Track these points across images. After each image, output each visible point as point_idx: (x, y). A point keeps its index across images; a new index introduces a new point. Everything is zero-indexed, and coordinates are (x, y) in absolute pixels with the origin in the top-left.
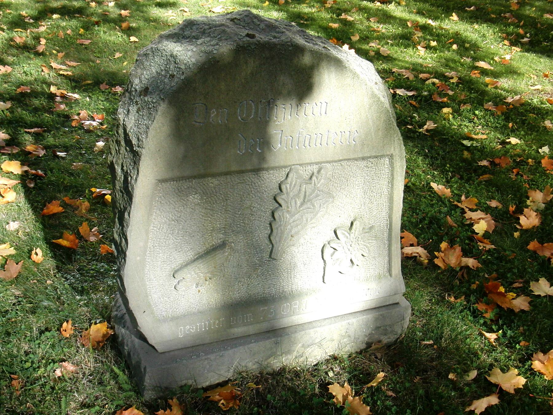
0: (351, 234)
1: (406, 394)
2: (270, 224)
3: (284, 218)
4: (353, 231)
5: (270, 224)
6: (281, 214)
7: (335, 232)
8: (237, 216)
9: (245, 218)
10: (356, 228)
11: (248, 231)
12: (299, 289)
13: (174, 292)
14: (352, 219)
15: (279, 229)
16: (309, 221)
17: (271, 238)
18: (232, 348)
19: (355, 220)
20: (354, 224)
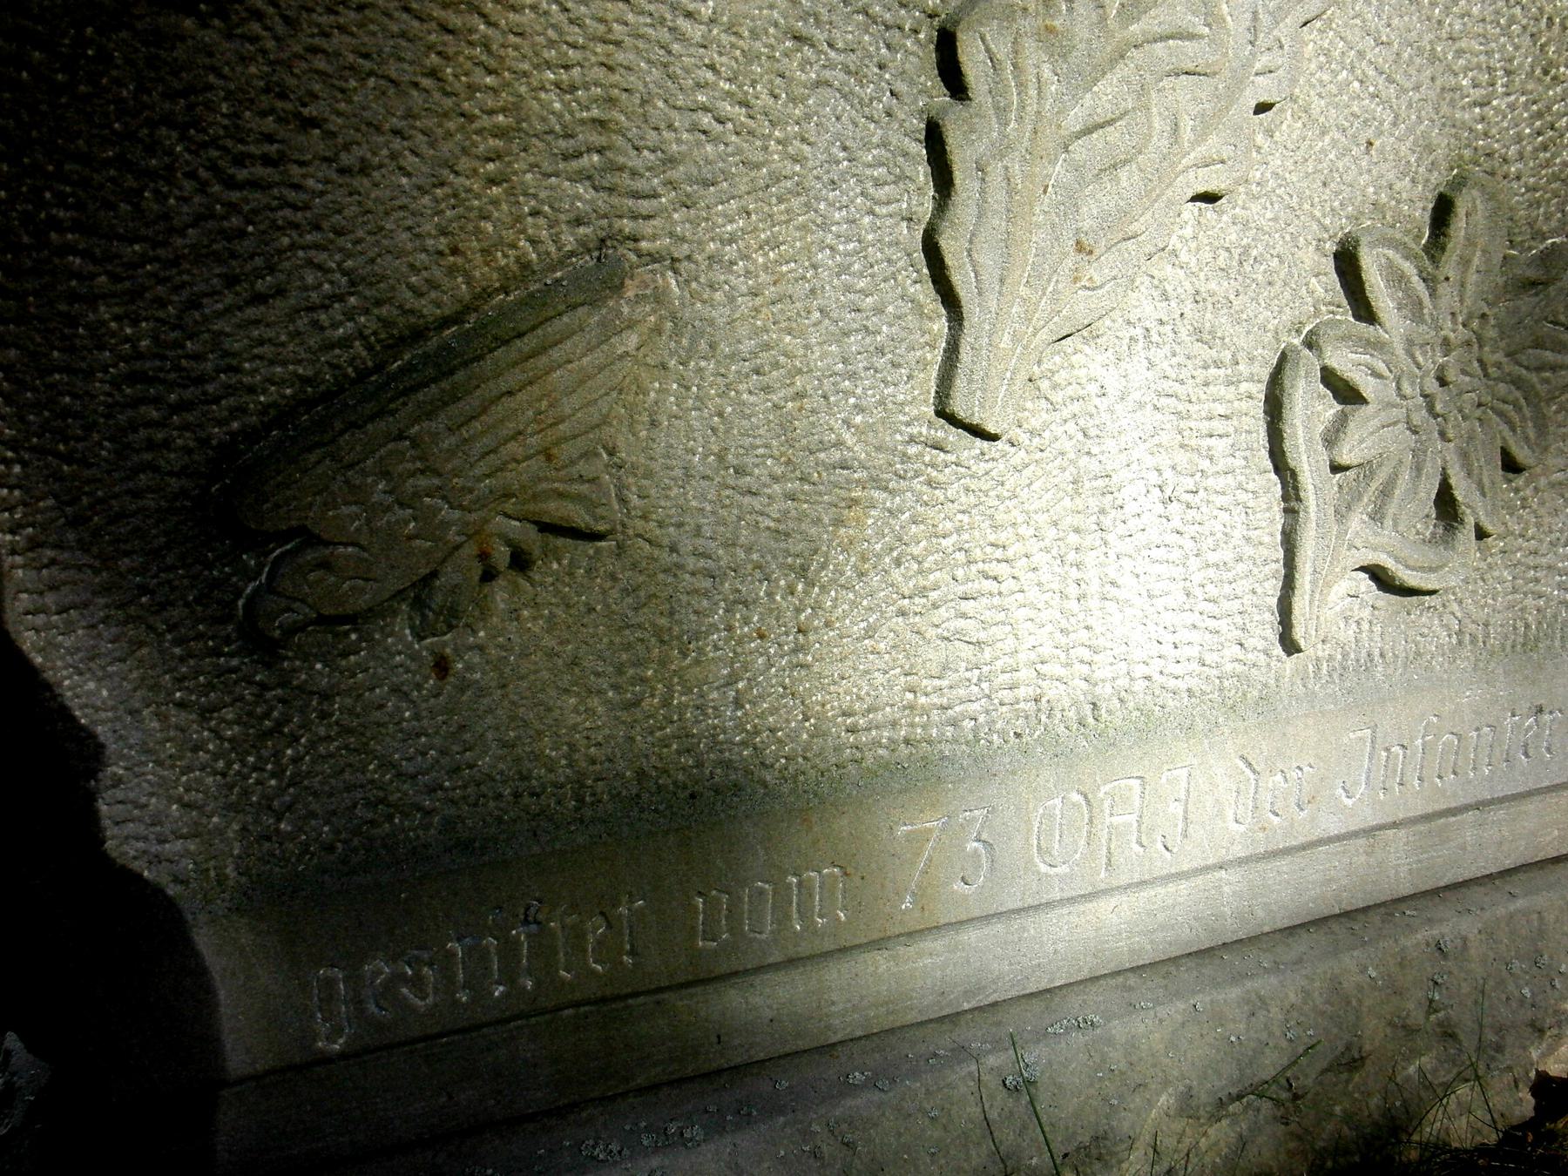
0: (1443, 289)
1: (776, 25)
2: (934, 138)
3: (1021, 86)
4: (1449, 266)
5: (934, 138)
6: (1002, 50)
7: (1347, 263)
8: (695, 32)
9: (750, 57)
10: (1470, 242)
11: (777, 178)
12: (836, 670)
13: (1290, 663)
14: (1438, 180)
15: (996, 170)
16: (1187, 134)
17: (949, 245)
18: (717, 1128)
19: (1459, 183)
20: (1461, 206)
